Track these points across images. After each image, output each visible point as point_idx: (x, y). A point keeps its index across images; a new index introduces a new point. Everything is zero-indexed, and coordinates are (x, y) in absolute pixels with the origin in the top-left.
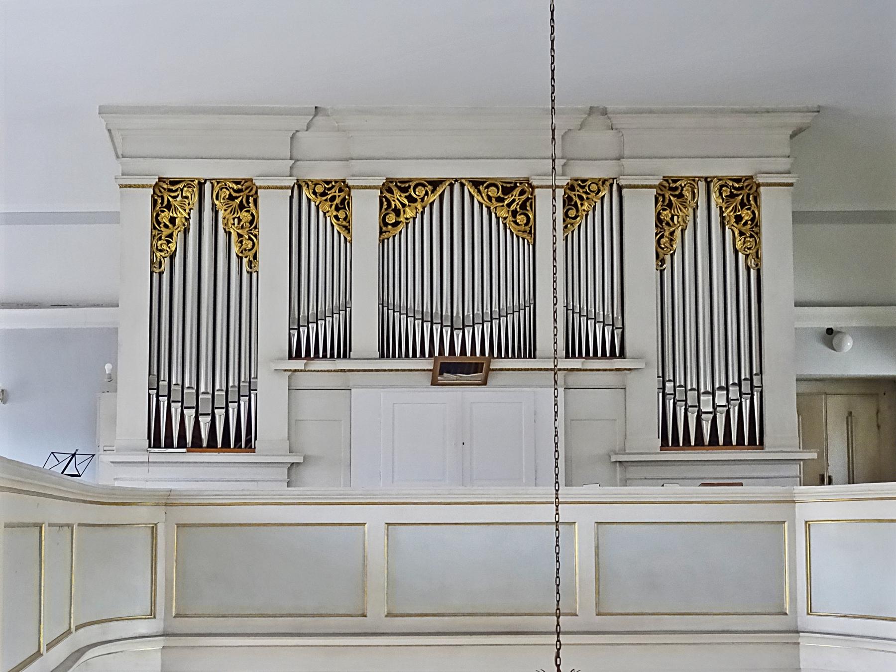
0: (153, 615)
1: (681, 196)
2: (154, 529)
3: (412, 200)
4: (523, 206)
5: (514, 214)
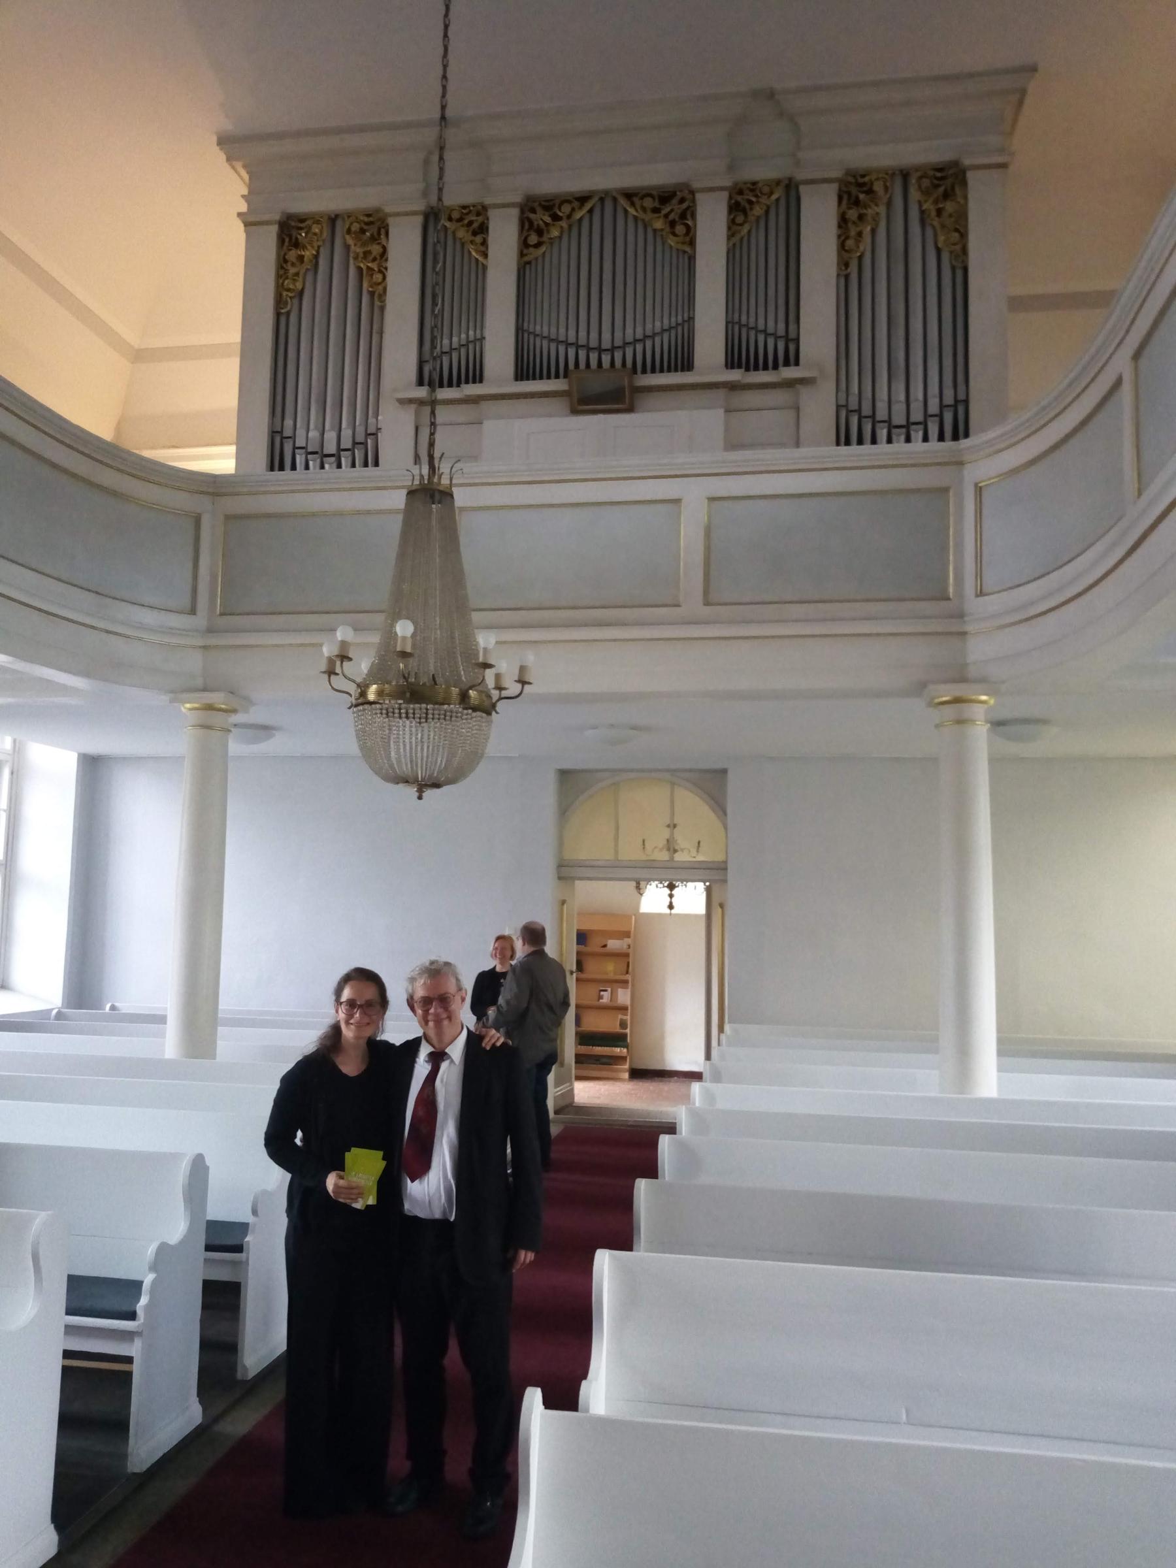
1: (870, 192)
3: (556, 218)
4: (683, 216)
5: (672, 224)
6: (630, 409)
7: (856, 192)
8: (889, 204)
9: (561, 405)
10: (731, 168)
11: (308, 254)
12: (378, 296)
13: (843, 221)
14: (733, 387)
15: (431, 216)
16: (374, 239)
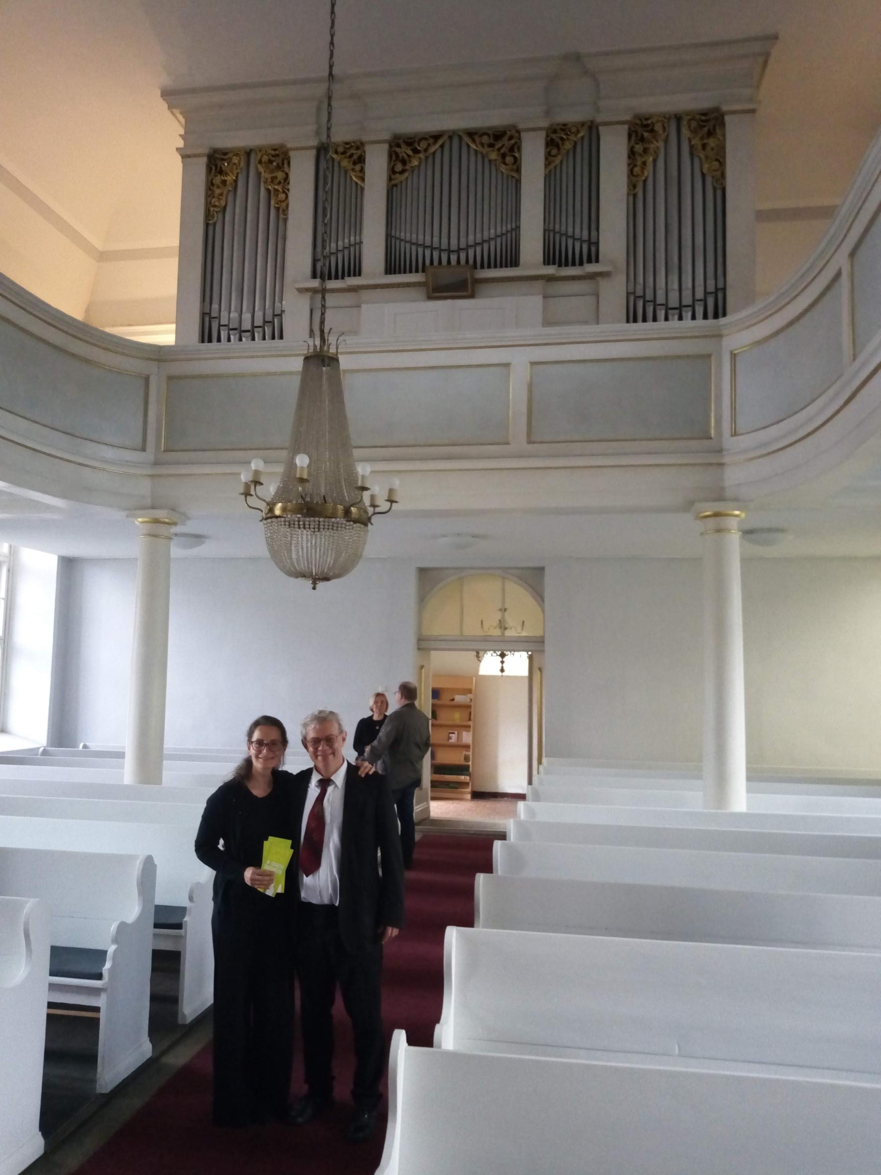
0: (143, 449)
1: (652, 131)
2: (147, 379)
3: (416, 151)
4: (512, 150)
5: (504, 156)
6: (472, 296)
7: (642, 131)
8: (666, 141)
9: (421, 293)
10: (548, 113)
11: (230, 178)
12: (282, 211)
13: (632, 154)
14: (550, 279)
15: (322, 150)
16: (279, 167)
